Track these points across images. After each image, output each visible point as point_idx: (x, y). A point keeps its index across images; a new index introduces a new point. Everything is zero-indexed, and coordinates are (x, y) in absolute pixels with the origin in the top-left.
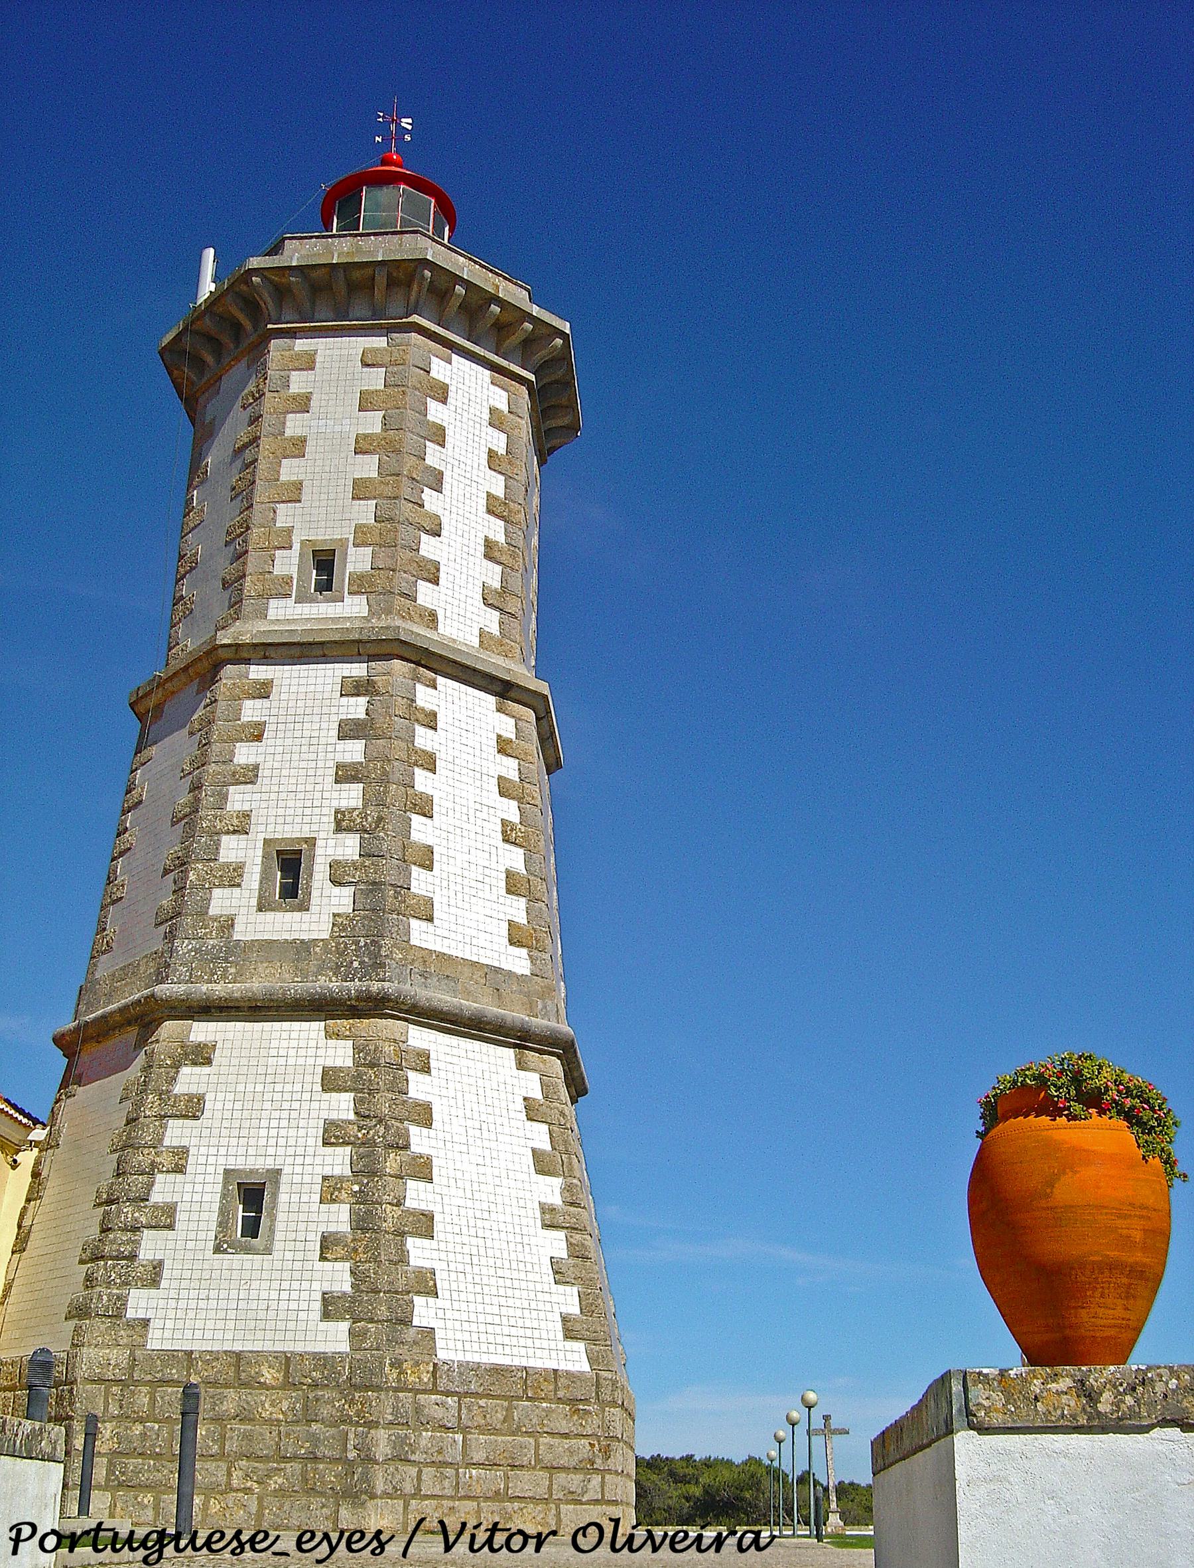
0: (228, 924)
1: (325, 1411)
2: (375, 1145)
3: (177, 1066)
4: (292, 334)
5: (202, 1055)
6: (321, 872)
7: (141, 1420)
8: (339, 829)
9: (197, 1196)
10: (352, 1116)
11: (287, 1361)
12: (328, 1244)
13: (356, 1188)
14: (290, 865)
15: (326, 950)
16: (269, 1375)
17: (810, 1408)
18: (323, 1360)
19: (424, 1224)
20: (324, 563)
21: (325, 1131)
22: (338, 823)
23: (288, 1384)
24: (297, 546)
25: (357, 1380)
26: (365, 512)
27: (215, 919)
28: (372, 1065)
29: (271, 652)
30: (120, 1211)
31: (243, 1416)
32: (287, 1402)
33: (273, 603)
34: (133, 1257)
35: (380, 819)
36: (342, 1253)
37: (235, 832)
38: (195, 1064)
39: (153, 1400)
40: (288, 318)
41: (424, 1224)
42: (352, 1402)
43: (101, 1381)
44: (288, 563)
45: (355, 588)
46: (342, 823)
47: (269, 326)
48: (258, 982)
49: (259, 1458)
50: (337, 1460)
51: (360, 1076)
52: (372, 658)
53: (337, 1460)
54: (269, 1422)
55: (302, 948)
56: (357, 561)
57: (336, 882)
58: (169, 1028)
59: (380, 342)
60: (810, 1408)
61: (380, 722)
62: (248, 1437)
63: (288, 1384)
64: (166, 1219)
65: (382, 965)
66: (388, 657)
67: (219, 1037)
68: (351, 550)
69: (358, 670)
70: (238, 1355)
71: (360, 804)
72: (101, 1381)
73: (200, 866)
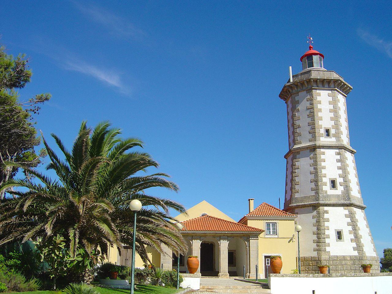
0: (326, 192)
1: (356, 263)
2: (355, 226)
3: (324, 214)
4: (316, 89)
5: (327, 212)
6: (338, 184)
7: (332, 265)
8: (340, 177)
9: (331, 233)
10: (351, 222)
11: (350, 257)
12: (352, 240)
13: (354, 232)
14: (333, 184)
15: (342, 196)
16: (348, 259)
17: (298, 232)
18: (355, 256)
19: (328, 220)
20: (327, 131)
21: (347, 224)
22: (339, 176)
23: (351, 260)
24: (323, 128)
25: (360, 259)
26: (333, 123)
27: (324, 191)
28: (351, 214)
29: (324, 147)
30: (321, 236)
31: (345, 264)
32: (351, 262)
33: (321, 138)
34: (325, 242)
35: (345, 176)
36: (354, 241)
37: (324, 177)
38: (326, 213)
39: (333, 262)
40: (326, 87)
41: (328, 220)
42: (360, 262)
43: (325, 260)
44: (322, 131)
45: (333, 136)
46: (340, 176)
47: (313, 88)
48: (332, 201)
49: (348, 270)
50: (359, 270)
51: (350, 215)
52: (339, 149)
53: (359, 270)
54: (349, 265)
55: (338, 196)
56: (332, 131)
57: (326, 183)
58: (321, 208)
59: (330, 92)
60: (298, 232)
61: (343, 160)
62: (347, 267)
63: (351, 260)
64: (328, 237)
65: (350, 199)
66: (341, 149)
67: (329, 209)
68: (332, 129)
69: (337, 151)
70: (344, 256)
71: (342, 173)
72: (325, 260)
73: (320, 182)
